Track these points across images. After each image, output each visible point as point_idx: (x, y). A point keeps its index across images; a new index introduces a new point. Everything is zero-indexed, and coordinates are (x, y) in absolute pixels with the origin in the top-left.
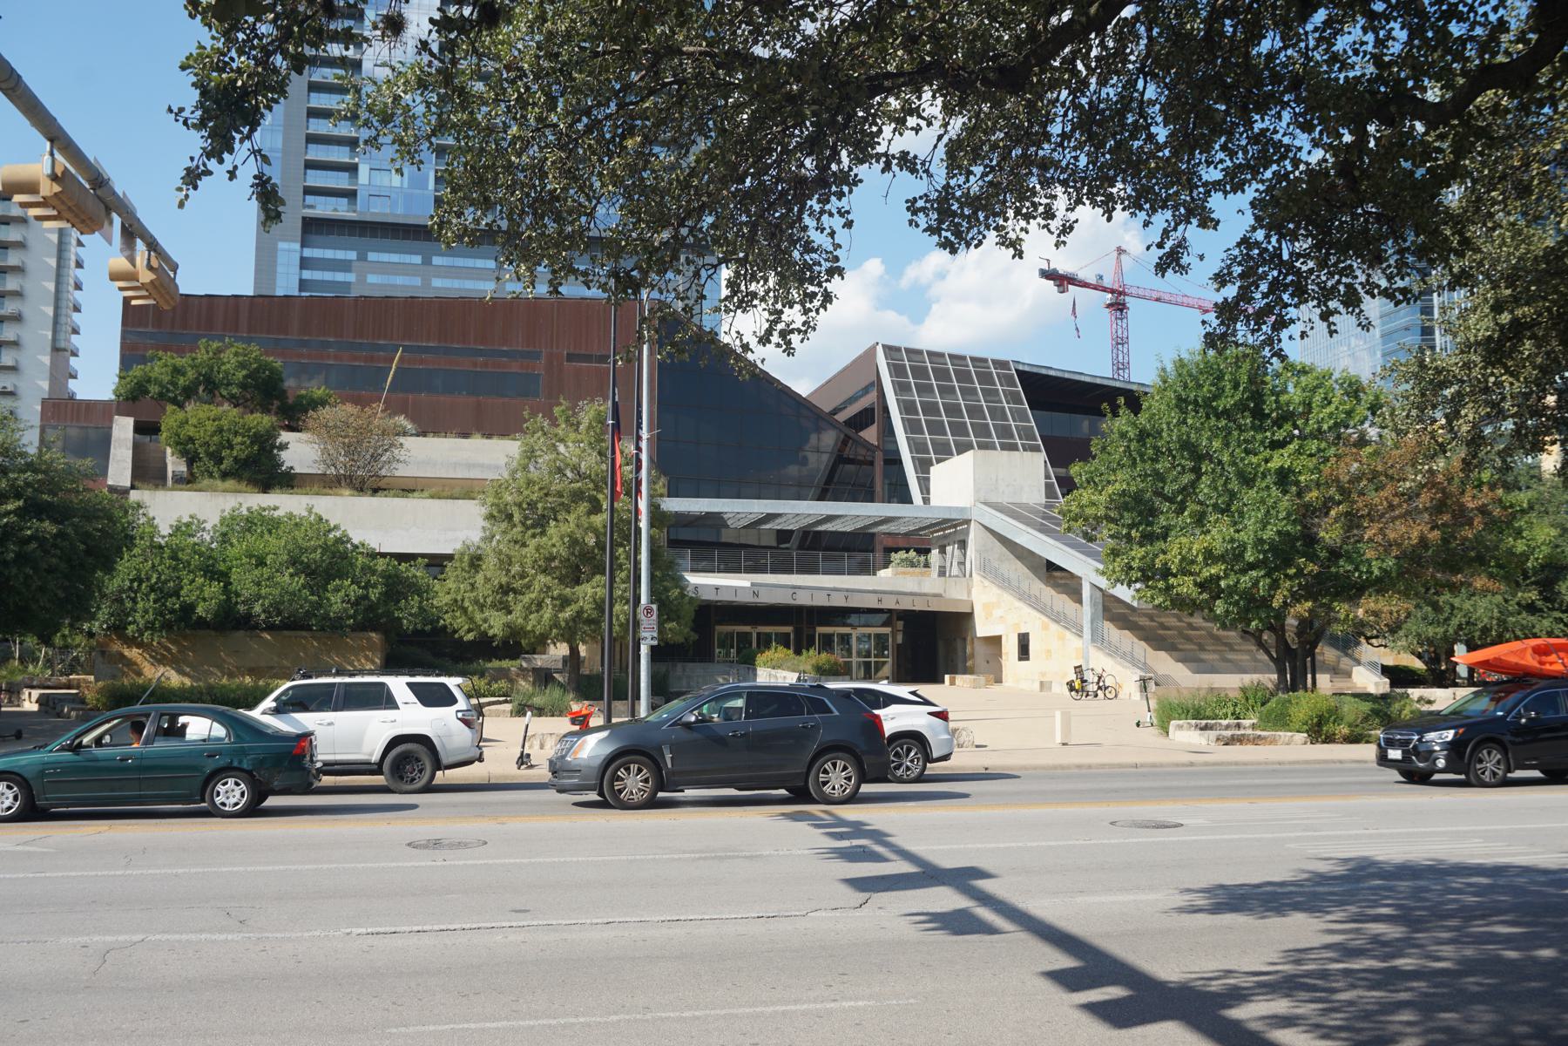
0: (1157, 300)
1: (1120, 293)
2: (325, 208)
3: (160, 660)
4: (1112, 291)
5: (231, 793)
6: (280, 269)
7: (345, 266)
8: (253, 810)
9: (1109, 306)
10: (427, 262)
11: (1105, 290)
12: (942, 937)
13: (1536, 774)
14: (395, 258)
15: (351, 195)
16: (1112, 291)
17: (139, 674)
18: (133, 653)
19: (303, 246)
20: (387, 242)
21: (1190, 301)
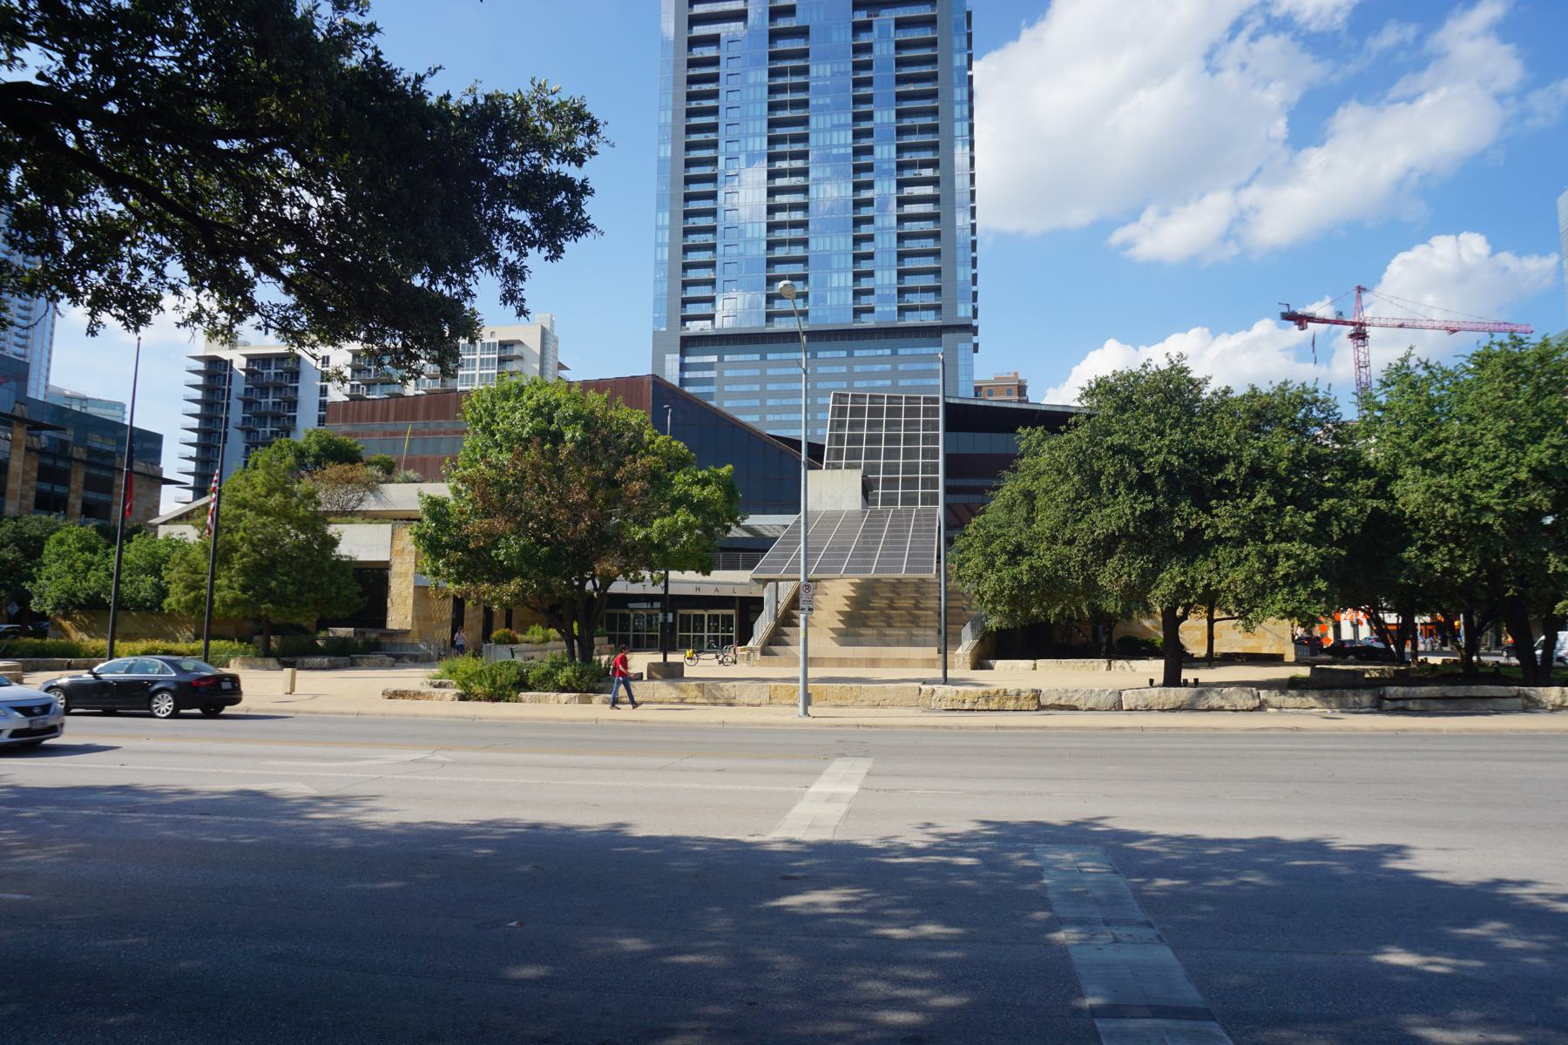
0: (1401, 326)
1: (1361, 324)
2: (695, 327)
3: (80, 629)
4: (1353, 324)
5: (165, 704)
6: (961, 362)
7: (710, 366)
8: (175, 715)
9: (1352, 336)
10: (763, 358)
11: (1345, 323)
12: (1531, 878)
13: (197, 711)
14: (872, 352)
15: (805, 314)
16: (1353, 324)
17: (69, 637)
18: (66, 624)
19: (683, 355)
20: (784, 345)
21: (1437, 324)
